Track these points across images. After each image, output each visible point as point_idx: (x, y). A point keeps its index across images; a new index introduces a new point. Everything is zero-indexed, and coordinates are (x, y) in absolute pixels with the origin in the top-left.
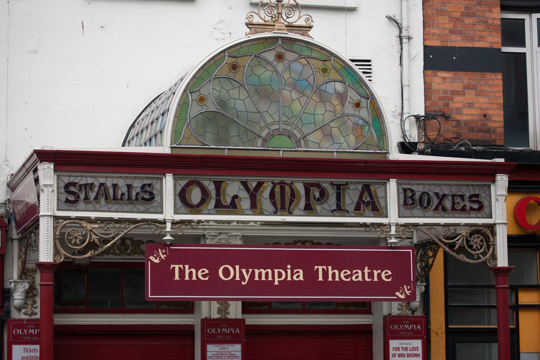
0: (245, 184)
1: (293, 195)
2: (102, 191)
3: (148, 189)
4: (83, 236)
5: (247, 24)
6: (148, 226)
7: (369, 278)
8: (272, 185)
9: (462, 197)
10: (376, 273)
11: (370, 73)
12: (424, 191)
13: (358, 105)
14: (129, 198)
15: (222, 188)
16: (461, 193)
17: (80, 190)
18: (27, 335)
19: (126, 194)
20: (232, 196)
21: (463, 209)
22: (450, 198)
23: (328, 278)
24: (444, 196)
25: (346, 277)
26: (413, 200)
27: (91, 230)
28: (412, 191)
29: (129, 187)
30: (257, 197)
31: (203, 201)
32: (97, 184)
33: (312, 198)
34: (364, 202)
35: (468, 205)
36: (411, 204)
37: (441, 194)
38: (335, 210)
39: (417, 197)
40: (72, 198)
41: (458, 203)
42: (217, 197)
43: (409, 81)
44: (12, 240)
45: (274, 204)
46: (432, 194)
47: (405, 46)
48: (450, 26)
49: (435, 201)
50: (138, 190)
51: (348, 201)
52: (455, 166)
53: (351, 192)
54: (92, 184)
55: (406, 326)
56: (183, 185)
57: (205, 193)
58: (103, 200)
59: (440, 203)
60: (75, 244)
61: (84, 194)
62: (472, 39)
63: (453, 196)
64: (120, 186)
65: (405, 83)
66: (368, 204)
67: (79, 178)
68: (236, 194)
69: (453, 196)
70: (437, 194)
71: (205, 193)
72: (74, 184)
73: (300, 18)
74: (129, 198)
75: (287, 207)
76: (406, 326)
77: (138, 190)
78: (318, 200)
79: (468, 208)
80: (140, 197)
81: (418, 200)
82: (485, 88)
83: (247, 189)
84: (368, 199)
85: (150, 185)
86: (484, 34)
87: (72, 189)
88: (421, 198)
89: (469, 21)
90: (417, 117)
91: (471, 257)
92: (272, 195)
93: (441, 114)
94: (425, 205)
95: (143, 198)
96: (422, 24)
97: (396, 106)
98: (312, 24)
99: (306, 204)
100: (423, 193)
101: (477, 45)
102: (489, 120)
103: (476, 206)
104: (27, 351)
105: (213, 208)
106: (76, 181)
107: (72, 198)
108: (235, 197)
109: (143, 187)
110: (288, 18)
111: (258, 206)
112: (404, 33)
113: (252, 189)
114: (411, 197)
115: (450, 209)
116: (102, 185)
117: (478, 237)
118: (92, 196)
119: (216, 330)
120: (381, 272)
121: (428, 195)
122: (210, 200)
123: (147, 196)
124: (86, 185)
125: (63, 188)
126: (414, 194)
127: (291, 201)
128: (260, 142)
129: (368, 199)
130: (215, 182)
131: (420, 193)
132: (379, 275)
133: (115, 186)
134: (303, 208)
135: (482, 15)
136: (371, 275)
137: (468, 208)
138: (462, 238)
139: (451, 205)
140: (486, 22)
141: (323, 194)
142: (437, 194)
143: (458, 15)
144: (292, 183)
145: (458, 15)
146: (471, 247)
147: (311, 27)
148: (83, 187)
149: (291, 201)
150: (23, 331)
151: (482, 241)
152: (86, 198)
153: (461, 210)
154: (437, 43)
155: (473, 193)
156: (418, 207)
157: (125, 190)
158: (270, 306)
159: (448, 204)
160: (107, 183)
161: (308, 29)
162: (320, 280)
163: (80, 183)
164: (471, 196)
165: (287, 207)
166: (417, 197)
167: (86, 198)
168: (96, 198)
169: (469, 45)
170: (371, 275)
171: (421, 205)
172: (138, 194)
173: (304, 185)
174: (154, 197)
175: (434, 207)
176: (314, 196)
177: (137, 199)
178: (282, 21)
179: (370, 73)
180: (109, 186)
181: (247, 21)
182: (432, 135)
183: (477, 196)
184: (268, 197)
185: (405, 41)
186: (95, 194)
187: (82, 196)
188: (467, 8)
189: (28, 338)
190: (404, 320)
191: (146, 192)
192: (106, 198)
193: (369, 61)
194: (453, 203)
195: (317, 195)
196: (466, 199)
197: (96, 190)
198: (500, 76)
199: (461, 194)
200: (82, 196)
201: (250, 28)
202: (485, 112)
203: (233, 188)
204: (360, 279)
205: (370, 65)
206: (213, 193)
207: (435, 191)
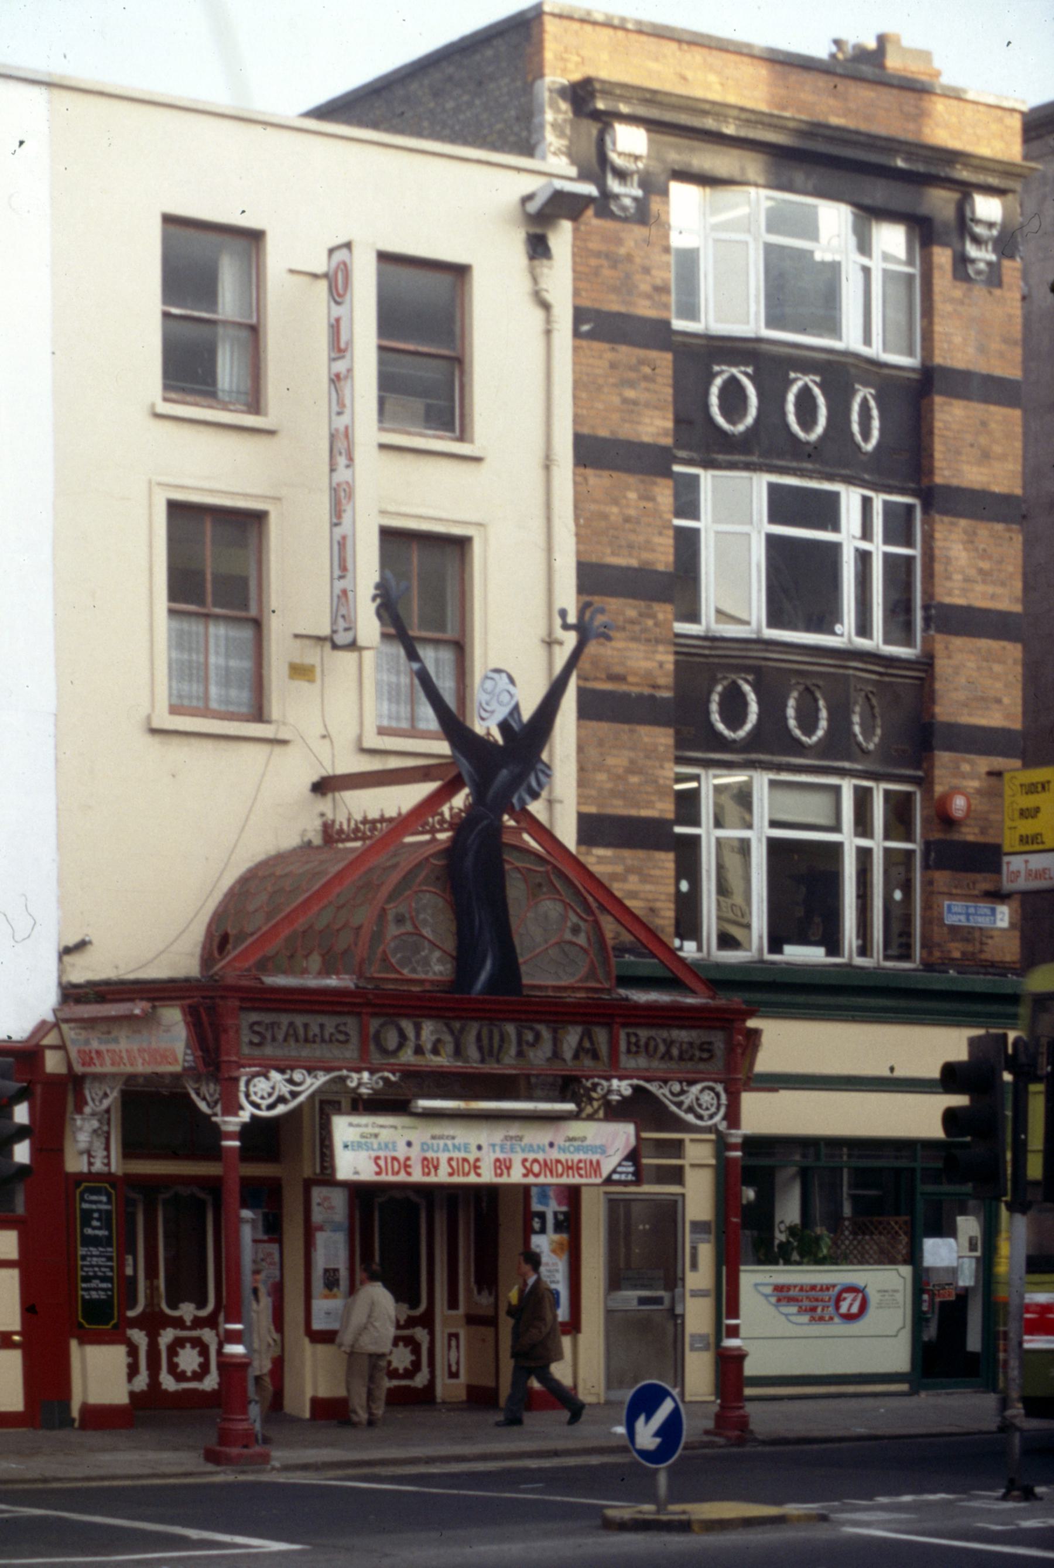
2: (291, 1032)
17: (267, 1029)
21: (691, 1059)
26: (638, 1046)
31: (401, 1046)
34: (583, 1049)
35: (697, 1053)
39: (642, 1042)
40: (256, 1040)
44: (1007, 1258)
46: (659, 1040)
48: (609, 785)
49: (662, 1048)
50: (332, 1030)
51: (565, 1047)
52: (908, 1089)
53: (569, 1038)
62: (637, 806)
66: (587, 1051)
70: (664, 1041)
77: (332, 1030)
82: (652, 872)
83: (452, 1032)
86: (653, 798)
88: (647, 1045)
89: (634, 779)
91: (700, 1117)
95: (338, 1041)
101: (645, 813)
102: (657, 916)
103: (705, 1055)
109: (337, 1026)
114: (637, 1045)
118: (280, 1037)
121: (655, 1040)
122: (408, 1043)
127: (500, 1047)
133: (306, 1026)
135: (650, 771)
140: (656, 782)
141: (538, 1036)
143: (620, 771)
145: (620, 771)
146: (700, 1106)
149: (500, 1047)
154: (592, 809)
156: (644, 1054)
159: (675, 1052)
166: (642, 1042)
167: (274, 1039)
168: (285, 1040)
169: (634, 812)
172: (331, 1035)
183: (710, 1043)
187: (269, 1036)
188: (632, 762)
191: (340, 1032)
198: (671, 856)
200: (269, 1036)
202: (651, 904)
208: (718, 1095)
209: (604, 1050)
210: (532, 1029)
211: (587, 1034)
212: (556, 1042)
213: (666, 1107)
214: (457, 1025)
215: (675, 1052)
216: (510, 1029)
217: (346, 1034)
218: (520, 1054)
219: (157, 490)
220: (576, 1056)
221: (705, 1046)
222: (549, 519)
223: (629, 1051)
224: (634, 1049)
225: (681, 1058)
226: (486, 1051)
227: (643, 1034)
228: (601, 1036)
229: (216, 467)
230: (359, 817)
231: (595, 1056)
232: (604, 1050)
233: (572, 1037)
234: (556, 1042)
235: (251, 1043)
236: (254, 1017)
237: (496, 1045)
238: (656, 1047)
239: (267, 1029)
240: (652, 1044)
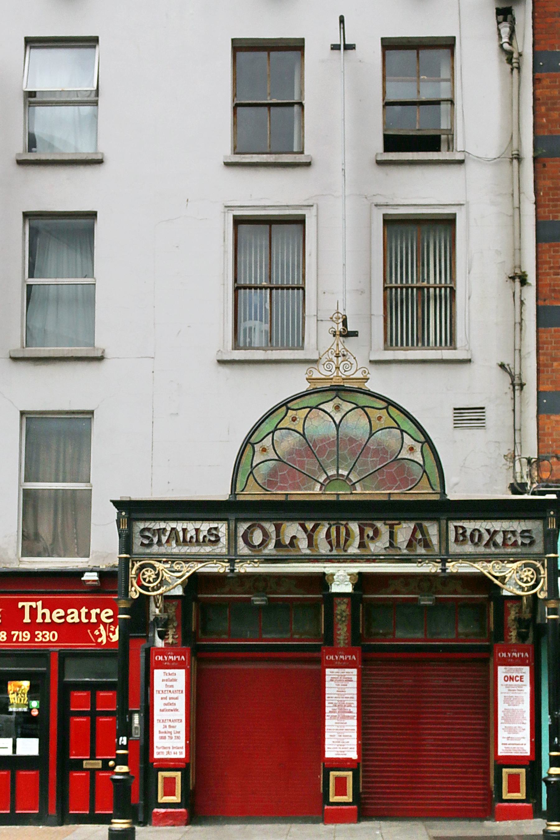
0: (303, 527)
1: (348, 533)
3: (214, 532)
4: (156, 575)
5: (307, 379)
6: (213, 565)
7: (86, 618)
8: (328, 526)
9: (513, 533)
10: (94, 612)
11: (484, 419)
12: (476, 527)
13: (411, 449)
14: (197, 541)
15: (282, 530)
16: (512, 529)
18: (167, 661)
19: (195, 537)
20: (291, 536)
21: (515, 544)
22: (501, 533)
23: (37, 618)
24: (496, 532)
25: (59, 618)
27: (162, 570)
28: (463, 528)
29: (197, 530)
30: (314, 537)
32: (169, 529)
33: (366, 537)
36: (463, 541)
37: (492, 530)
38: (388, 548)
39: (468, 533)
40: (146, 542)
41: (510, 539)
42: (276, 537)
43: (521, 425)
45: (330, 543)
46: (483, 531)
47: (517, 393)
49: (486, 537)
54: (164, 529)
55: (514, 654)
56: (245, 528)
57: (266, 534)
58: (174, 543)
59: (491, 539)
60: (149, 582)
61: (157, 537)
63: (504, 532)
64: (189, 530)
65: (517, 427)
67: (153, 524)
68: (294, 535)
69: (504, 532)
71: (266, 534)
72: (148, 529)
73: (357, 370)
74: (197, 541)
75: (342, 546)
76: (514, 654)
77: (205, 533)
78: (372, 538)
79: (520, 543)
80: (207, 539)
81: (469, 537)
84: (420, 537)
85: (216, 529)
87: (147, 534)
88: (472, 535)
90: (529, 461)
92: (328, 535)
93: (554, 455)
94: (476, 540)
96: (536, 370)
97: (509, 450)
98: (368, 376)
99: (360, 543)
100: (474, 530)
103: (527, 541)
104: (167, 675)
105: (273, 547)
106: (150, 527)
107: (146, 542)
108: (294, 537)
109: (209, 530)
110: (345, 371)
111: (296, 545)
112: (517, 381)
113: (309, 530)
114: (463, 534)
115: (501, 545)
116: (173, 529)
117: (529, 571)
118: (164, 539)
119: (334, 657)
120: (101, 611)
123: (213, 539)
124: (159, 530)
125: (138, 534)
126: (465, 531)
127: (346, 541)
128: (318, 486)
129: (420, 537)
130: (274, 524)
131: (472, 530)
132: (98, 616)
133: (184, 530)
134: (357, 546)
136: (88, 616)
137: (520, 543)
138: (513, 571)
139: (502, 540)
141: (377, 532)
142: (488, 531)
144: (347, 524)
147: (368, 379)
148: (156, 531)
149: (346, 541)
150: (164, 658)
151: (533, 574)
152: (159, 541)
153: (511, 545)
155: (525, 529)
156: (470, 543)
157: (193, 533)
158: (394, 636)
159: (499, 539)
160: (177, 528)
161: (365, 380)
162: (25, 621)
163: (155, 528)
164: (523, 532)
165: (342, 546)
166: (468, 533)
167: (159, 541)
168: (168, 541)
170: (88, 616)
171: (472, 541)
172: (205, 536)
173: (359, 526)
174: (219, 540)
175: (484, 542)
176: (368, 536)
177: (190, 541)
178: (340, 374)
179: (484, 419)
180: (179, 530)
181: (307, 376)
182: (545, 475)
183: (528, 531)
184: (325, 536)
185: (517, 387)
186: (167, 538)
189: (168, 664)
190: (511, 649)
192: (177, 541)
193: (483, 408)
194: (505, 539)
195: (371, 534)
196: (518, 535)
197: (168, 534)
199: (513, 529)
200: (156, 540)
201: (309, 382)
203: (292, 529)
204: (77, 620)
205: (484, 412)
206: (274, 535)
207: (487, 528)
208: (537, 571)
209: (435, 540)
210: (372, 526)
211: (419, 528)
212: (392, 535)
213: (492, 582)
214: (310, 525)
215: (499, 539)
216: (354, 527)
217: (217, 536)
218: (362, 545)
219: (375, 209)
220: (410, 545)
221: (526, 534)
222: (461, 73)
223: (456, 540)
224: (461, 538)
225: (505, 544)
226: (334, 542)
227: (470, 526)
228: (433, 530)
229: (269, 191)
230: (112, 564)
231: (427, 544)
232: (435, 540)
233: (404, 531)
234: (392, 535)
235: (142, 544)
236: (141, 525)
237: (342, 542)
238: (480, 536)
239: (154, 535)
240: (477, 534)
